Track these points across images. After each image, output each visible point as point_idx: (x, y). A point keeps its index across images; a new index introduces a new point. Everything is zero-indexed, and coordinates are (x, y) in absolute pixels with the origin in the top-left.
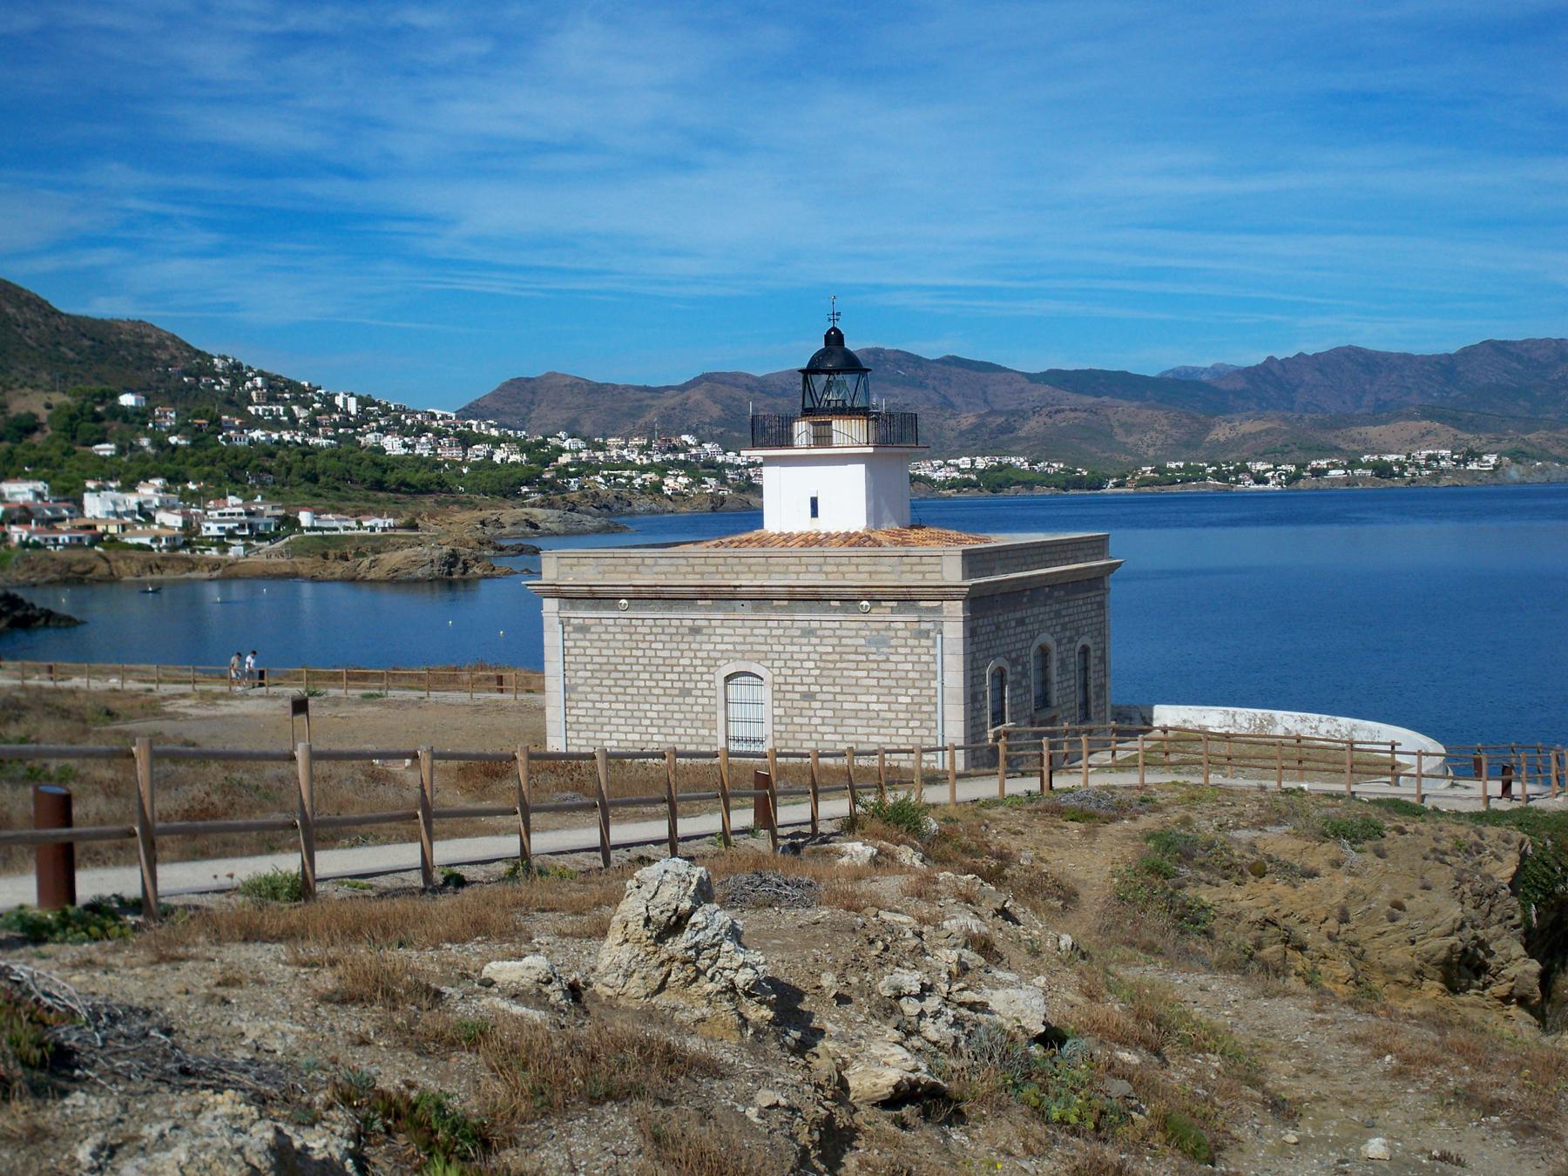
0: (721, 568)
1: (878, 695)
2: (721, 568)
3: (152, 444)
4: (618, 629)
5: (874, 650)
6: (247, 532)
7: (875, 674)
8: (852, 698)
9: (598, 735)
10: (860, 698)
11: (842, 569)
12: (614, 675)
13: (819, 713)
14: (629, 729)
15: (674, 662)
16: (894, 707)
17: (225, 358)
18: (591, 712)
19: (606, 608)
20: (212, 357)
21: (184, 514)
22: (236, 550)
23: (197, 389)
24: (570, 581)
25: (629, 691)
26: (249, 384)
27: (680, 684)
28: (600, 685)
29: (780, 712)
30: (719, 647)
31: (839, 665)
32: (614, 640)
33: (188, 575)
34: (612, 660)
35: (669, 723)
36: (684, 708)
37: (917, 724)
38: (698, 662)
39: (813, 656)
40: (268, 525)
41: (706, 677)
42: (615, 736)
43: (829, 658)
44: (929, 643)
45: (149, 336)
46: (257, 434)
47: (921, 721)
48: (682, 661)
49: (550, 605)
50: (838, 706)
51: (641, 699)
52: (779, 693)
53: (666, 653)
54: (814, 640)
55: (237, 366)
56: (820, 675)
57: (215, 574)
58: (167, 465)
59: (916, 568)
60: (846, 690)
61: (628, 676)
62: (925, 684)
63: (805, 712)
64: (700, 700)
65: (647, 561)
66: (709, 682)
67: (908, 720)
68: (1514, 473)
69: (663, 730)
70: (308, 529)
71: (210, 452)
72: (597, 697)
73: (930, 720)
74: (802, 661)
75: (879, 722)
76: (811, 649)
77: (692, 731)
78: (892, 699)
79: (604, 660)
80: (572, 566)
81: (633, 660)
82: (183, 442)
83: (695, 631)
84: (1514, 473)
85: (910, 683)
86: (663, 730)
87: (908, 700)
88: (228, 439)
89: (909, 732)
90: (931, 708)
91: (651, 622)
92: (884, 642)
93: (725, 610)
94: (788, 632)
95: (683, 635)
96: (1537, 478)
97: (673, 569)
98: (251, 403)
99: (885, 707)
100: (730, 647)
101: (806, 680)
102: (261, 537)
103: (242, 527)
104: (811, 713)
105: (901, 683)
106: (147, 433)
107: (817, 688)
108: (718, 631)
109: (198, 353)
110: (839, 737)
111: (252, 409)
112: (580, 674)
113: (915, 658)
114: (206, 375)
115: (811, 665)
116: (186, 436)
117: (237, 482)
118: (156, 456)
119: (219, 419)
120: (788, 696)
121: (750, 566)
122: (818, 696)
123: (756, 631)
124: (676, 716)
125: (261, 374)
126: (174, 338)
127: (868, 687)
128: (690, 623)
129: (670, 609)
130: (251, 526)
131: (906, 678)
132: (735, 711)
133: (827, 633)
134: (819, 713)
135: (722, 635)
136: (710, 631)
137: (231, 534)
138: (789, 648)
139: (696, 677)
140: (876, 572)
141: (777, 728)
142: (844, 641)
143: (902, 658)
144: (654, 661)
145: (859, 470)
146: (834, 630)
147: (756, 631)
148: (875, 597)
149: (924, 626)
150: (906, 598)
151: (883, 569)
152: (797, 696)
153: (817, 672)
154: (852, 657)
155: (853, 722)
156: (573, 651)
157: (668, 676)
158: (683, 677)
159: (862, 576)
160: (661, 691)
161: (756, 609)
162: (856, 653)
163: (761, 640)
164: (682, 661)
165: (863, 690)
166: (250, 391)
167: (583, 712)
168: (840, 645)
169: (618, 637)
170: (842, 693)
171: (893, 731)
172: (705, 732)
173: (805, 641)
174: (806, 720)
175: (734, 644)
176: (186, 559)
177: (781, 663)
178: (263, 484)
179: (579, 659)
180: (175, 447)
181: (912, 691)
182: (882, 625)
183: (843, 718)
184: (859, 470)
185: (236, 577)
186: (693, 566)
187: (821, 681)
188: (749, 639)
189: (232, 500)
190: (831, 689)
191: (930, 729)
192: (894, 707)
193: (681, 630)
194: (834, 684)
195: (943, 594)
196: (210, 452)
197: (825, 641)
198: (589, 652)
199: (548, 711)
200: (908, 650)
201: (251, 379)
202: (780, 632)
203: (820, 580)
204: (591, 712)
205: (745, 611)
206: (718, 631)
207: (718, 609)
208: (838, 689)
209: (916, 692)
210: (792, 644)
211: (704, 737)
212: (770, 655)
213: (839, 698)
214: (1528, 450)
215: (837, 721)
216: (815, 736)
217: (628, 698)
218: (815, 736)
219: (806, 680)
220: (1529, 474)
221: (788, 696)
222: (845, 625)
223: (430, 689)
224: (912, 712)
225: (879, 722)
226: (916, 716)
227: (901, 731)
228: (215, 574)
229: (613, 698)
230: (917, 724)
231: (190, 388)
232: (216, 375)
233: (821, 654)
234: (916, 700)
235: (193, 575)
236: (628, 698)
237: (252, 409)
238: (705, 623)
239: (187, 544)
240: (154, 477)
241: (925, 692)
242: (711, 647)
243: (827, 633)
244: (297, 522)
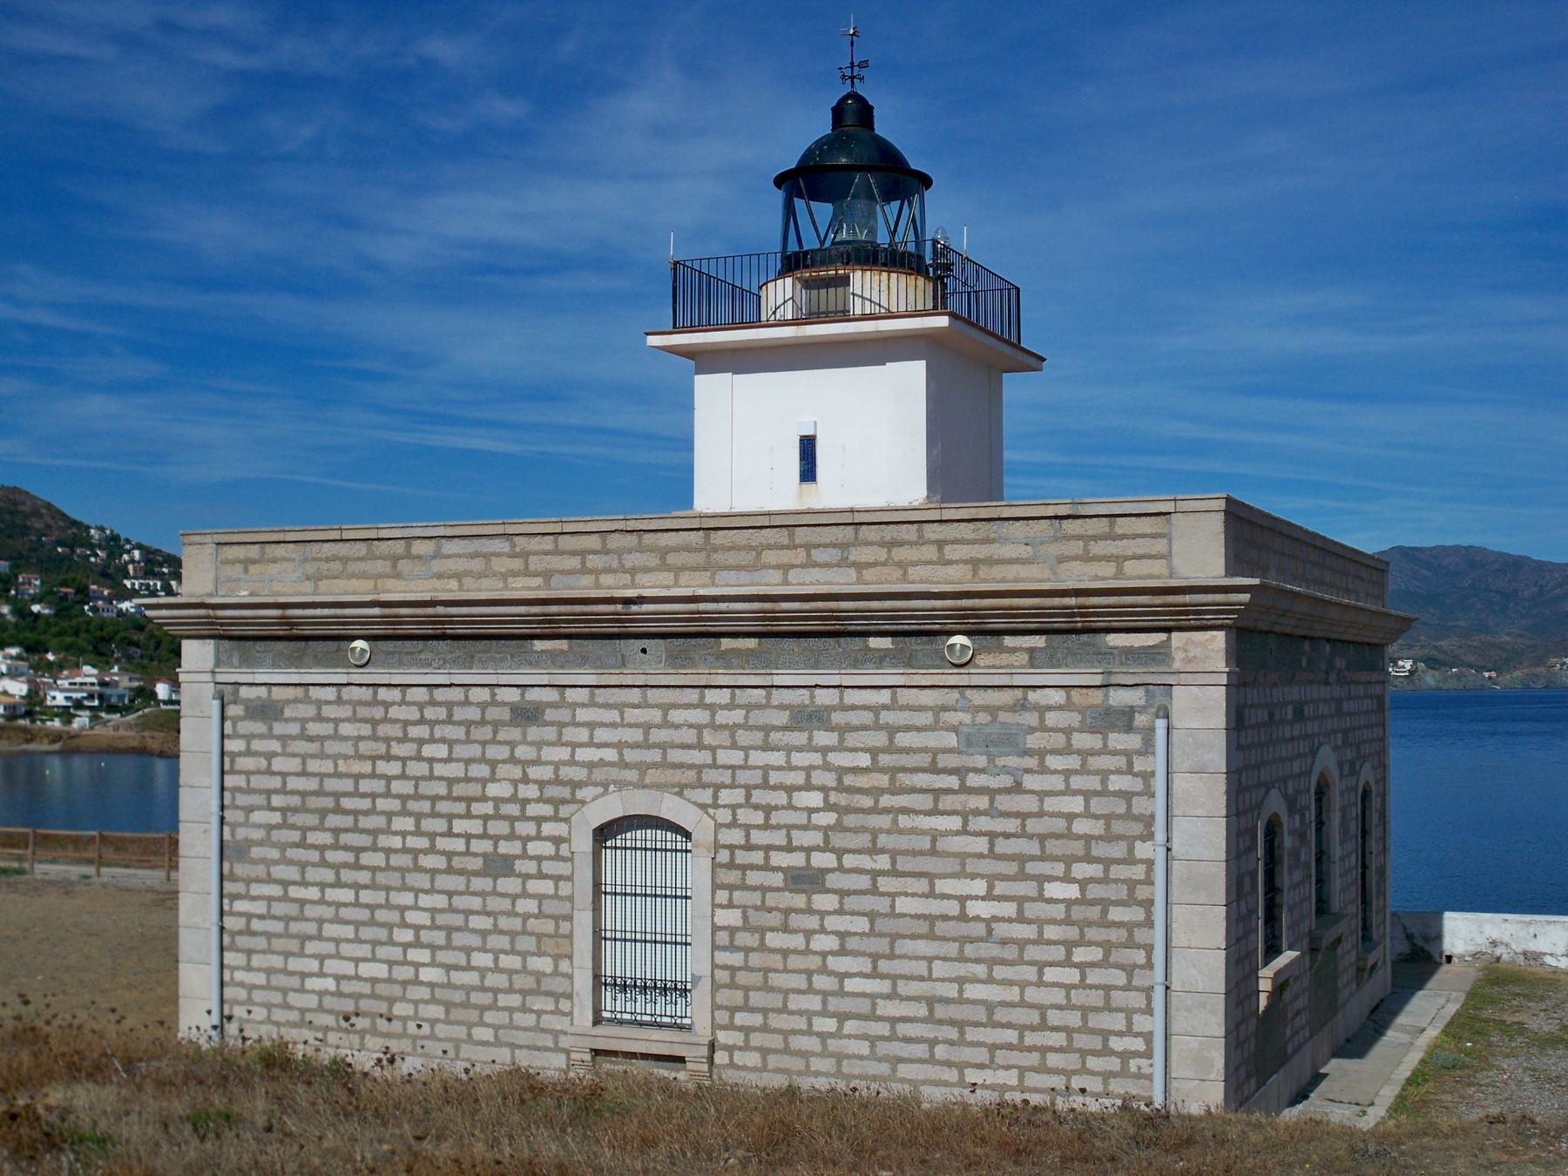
0: (593, 561)
1: (991, 879)
2: (593, 561)
3: (13, 612)
4: (346, 712)
5: (981, 761)
6: (96, 703)
7: (983, 823)
8: (922, 885)
9: (295, 964)
10: (942, 886)
11: (900, 554)
12: (333, 821)
13: (832, 923)
14: (365, 950)
15: (473, 790)
16: (1032, 910)
17: (102, 529)
18: (279, 909)
19: (320, 662)
20: (88, 528)
21: (29, 682)
22: (81, 721)
23: (71, 560)
24: (243, 596)
25: (368, 859)
26: (126, 557)
27: (484, 846)
28: (302, 844)
29: (731, 917)
30: (583, 755)
31: (886, 801)
32: (335, 736)
33: (25, 746)
34: (332, 785)
35: (459, 939)
36: (494, 904)
37: (1096, 954)
38: (531, 791)
39: (819, 778)
40: (121, 697)
41: (549, 829)
42: (332, 966)
43: (862, 781)
44: (1134, 741)
45: (24, 503)
46: (126, 605)
47: (1107, 947)
48: (493, 790)
49: (196, 654)
50: (882, 905)
51: (393, 879)
52: (729, 871)
53: (455, 770)
54: (823, 738)
55: (115, 538)
56: (839, 827)
57: (56, 747)
58: (28, 634)
59: (1097, 548)
60: (904, 864)
61: (365, 822)
62: (1118, 850)
63: (795, 920)
64: (534, 886)
65: (419, 548)
66: (557, 841)
67: (1070, 945)
68: (1430, 679)
69: (444, 957)
70: (165, 703)
71: (74, 622)
72: (292, 873)
73: (1130, 944)
74: (790, 790)
75: (993, 950)
76: (815, 759)
77: (513, 962)
78: (1029, 888)
79: (311, 784)
80: (247, 563)
81: (379, 786)
82: (46, 611)
83: (527, 715)
84: (1430, 679)
85: (1077, 848)
86: (444, 957)
87: (1073, 891)
88: (95, 609)
89: (1073, 976)
90: (1137, 914)
91: (420, 695)
92: (1009, 741)
93: (599, 664)
94: (758, 718)
95: (497, 725)
96: (1452, 684)
97: (477, 565)
98: (127, 576)
99: (1009, 909)
100: (610, 755)
101: (801, 838)
102: (112, 709)
103: (91, 697)
104: (812, 922)
105: (1053, 847)
106: (8, 601)
107: (828, 860)
108: (583, 715)
109: (75, 523)
110: (883, 986)
111: (128, 583)
112: (257, 817)
113: (1093, 783)
114: (81, 546)
115: (815, 799)
116: (49, 604)
117: (101, 654)
118: (16, 626)
119: (87, 588)
120: (754, 878)
121: (664, 552)
122: (832, 880)
123: (676, 716)
124: (477, 922)
125: (139, 547)
126: (49, 506)
127: (963, 857)
128: (512, 695)
129: (468, 662)
130: (101, 697)
131: (1069, 835)
132: (615, 914)
133: (856, 718)
134: (832, 923)
135: (592, 726)
136: (563, 715)
137: (79, 705)
138: (758, 758)
139: (527, 828)
140: (990, 562)
141: (723, 958)
142: (903, 739)
143: (1057, 783)
144: (427, 788)
145: (912, 375)
146: (875, 709)
147: (676, 716)
148: (987, 621)
149: (1119, 698)
150: (1070, 622)
151: (1007, 551)
152: (777, 879)
153: (829, 818)
154: (921, 780)
155: (922, 947)
156: (245, 763)
157: (459, 826)
158: (497, 827)
159: (954, 572)
160: (440, 862)
161: (675, 661)
162: (934, 769)
163: (689, 736)
164: (493, 790)
165: (952, 865)
166: (127, 563)
167: (259, 908)
168: (891, 749)
169: (347, 729)
170: (894, 873)
171: (1030, 973)
172: (544, 964)
173: (799, 738)
174: (797, 941)
175: (619, 746)
176: (24, 730)
177: (737, 796)
178: (129, 658)
179: (256, 782)
180: (38, 616)
181: (1081, 870)
182: (1006, 697)
183: (894, 937)
184: (912, 375)
185: (77, 751)
186: (525, 555)
187: (838, 840)
188: (658, 736)
189: (87, 669)
190: (865, 862)
191: (1129, 969)
192: (1032, 910)
193: (493, 713)
194: (873, 851)
195: (1175, 610)
196: (74, 622)
197: (852, 739)
198: (278, 764)
199: (185, 903)
200: (1073, 762)
201: (129, 552)
202: (737, 716)
203: (843, 581)
204: (279, 909)
205: (649, 664)
206: (583, 715)
207: (584, 661)
208: (883, 862)
209: (1095, 870)
210: (766, 747)
211: (539, 975)
212: (711, 776)
213: (884, 884)
214: (1440, 657)
215: (882, 945)
216: (820, 982)
217: (364, 877)
218: (820, 982)
219: (801, 838)
220: (1445, 681)
221: (754, 878)
222: (905, 696)
223: (101, 862)
224: (1084, 924)
225: (993, 950)
226: (1092, 933)
227: (1051, 974)
228: (56, 747)
229: (328, 875)
230: (1096, 954)
231: (63, 558)
232: (92, 547)
233: (842, 771)
234: (1095, 891)
235: (32, 747)
236: (364, 877)
237: (128, 583)
238: (551, 695)
239: (29, 713)
240: (12, 645)
241: (1118, 871)
242: (563, 753)
243: (856, 718)
244: (154, 695)
